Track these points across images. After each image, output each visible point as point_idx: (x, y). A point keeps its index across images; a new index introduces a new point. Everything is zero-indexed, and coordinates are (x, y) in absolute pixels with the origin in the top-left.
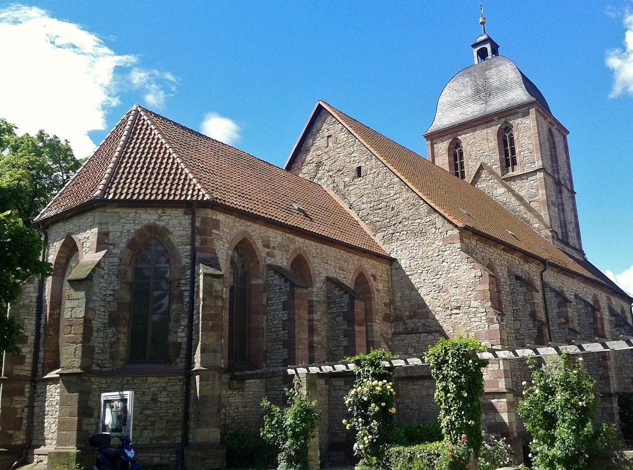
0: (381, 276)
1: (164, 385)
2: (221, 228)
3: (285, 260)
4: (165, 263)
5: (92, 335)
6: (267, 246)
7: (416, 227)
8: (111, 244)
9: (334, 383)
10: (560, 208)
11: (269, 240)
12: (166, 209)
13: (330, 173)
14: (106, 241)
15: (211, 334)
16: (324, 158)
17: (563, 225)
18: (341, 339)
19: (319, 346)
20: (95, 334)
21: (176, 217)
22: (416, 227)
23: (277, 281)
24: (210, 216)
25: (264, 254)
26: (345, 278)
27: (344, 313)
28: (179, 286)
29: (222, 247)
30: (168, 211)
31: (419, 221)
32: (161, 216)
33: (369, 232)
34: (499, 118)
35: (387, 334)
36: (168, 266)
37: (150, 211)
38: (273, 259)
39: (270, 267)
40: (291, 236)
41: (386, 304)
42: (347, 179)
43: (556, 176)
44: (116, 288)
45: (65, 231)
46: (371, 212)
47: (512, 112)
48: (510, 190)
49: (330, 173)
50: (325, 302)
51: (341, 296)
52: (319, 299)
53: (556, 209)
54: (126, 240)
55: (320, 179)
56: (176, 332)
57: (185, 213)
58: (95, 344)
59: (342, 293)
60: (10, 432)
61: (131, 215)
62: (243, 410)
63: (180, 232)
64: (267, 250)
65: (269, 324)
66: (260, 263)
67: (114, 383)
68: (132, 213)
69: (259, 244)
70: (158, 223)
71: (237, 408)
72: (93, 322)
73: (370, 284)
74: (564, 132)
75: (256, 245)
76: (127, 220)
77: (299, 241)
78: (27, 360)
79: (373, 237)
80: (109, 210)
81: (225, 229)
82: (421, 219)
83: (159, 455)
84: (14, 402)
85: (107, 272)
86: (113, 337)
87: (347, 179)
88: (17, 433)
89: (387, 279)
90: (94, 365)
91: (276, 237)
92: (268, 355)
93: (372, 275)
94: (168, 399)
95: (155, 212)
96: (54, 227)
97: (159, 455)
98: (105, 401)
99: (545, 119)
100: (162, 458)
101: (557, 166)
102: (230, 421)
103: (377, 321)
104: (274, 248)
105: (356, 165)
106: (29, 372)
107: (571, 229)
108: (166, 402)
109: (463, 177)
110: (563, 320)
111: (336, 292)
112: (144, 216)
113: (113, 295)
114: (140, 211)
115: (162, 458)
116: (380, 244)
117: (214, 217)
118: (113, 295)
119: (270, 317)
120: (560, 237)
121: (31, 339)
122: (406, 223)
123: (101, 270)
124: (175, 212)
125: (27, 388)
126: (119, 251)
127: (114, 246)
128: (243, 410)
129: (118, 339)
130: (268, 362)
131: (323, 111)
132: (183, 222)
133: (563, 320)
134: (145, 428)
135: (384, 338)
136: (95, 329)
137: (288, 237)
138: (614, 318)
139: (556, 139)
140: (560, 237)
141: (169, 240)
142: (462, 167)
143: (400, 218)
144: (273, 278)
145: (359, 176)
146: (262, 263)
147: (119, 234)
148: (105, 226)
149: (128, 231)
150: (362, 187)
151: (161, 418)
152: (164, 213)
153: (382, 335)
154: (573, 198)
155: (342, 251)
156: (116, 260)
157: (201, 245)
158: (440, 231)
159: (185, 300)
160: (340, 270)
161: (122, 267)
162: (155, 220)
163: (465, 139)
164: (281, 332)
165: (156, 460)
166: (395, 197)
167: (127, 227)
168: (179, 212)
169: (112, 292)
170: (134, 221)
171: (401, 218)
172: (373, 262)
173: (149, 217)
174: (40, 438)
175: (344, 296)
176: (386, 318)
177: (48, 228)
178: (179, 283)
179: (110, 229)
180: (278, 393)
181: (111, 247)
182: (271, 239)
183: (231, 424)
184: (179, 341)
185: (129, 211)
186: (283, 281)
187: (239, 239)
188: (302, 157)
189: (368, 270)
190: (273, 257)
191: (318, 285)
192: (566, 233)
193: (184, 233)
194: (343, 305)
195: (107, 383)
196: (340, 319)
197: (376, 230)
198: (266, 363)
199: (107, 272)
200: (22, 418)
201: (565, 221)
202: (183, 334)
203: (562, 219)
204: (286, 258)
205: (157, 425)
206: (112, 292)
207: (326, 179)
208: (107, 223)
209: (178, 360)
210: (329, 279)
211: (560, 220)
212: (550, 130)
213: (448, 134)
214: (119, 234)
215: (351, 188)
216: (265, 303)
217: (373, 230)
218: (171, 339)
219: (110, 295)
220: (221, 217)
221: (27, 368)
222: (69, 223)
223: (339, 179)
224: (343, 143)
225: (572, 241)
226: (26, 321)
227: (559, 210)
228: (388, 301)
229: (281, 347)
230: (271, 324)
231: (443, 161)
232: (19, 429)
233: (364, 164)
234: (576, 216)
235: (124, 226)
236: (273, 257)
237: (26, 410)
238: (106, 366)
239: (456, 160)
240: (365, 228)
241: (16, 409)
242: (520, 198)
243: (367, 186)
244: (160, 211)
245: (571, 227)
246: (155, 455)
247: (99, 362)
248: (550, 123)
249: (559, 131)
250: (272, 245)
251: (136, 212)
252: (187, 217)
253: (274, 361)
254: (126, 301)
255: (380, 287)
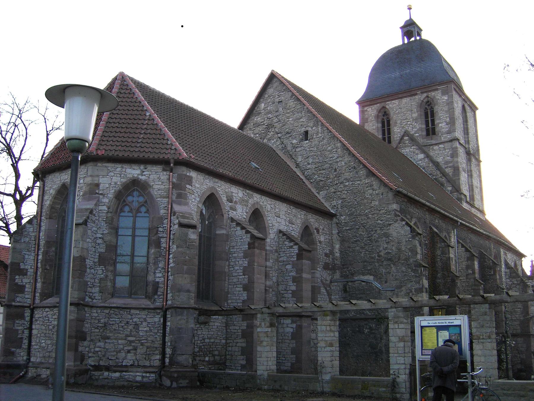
0: (323, 230)
1: (144, 317)
2: (193, 184)
3: (245, 213)
4: (145, 212)
5: (86, 272)
6: (230, 200)
7: (355, 188)
8: (101, 194)
9: (282, 322)
10: (469, 174)
11: (232, 196)
12: (147, 166)
13: (279, 135)
14: (97, 191)
15: (186, 276)
16: (275, 121)
17: (471, 189)
18: (290, 284)
19: (271, 290)
20: (88, 270)
21: (156, 172)
22: (355, 188)
23: (239, 232)
24: (184, 173)
25: (228, 208)
26: (293, 230)
27: (293, 261)
28: (157, 233)
29: (193, 200)
30: (149, 167)
31: (359, 182)
32: (144, 172)
33: (314, 190)
34: (422, 93)
35: (326, 280)
36: (148, 215)
37: (135, 167)
38: (235, 213)
39: (232, 220)
40: (251, 193)
41: (326, 255)
42: (294, 141)
43: (467, 146)
44: (105, 232)
45: (61, 180)
46: (315, 172)
47: (413, 93)
48: (428, 156)
49: (279, 135)
50: (276, 251)
51: (291, 247)
52: (272, 249)
53: (466, 175)
54: (113, 191)
55: (269, 140)
56: (155, 273)
57: (164, 170)
58: (88, 280)
59: (292, 244)
60: (13, 349)
61: (118, 169)
62: (208, 341)
63: (159, 186)
64: (230, 204)
65: (230, 269)
66: (225, 215)
67: (103, 312)
68: (119, 168)
69: (224, 199)
70: (140, 177)
71: (204, 339)
72: (87, 260)
73: (314, 236)
74: (474, 108)
75: (222, 199)
76: (115, 174)
77: (257, 198)
78: (26, 290)
79: (317, 195)
80: (99, 164)
81: (197, 185)
82: (360, 181)
83: (141, 374)
84: (16, 325)
85: (97, 218)
86: (102, 274)
87: (294, 141)
88: (18, 351)
89: (328, 233)
90: (87, 297)
91: (238, 193)
92: (229, 296)
93: (316, 229)
94: (148, 329)
95: (138, 168)
96: (50, 177)
97: (141, 374)
98: (340, 375)
99: (460, 96)
100: (143, 377)
101: (465, 138)
102: (198, 349)
103: (318, 269)
104: (236, 203)
105: (303, 129)
106: (29, 300)
107: (477, 192)
108: (146, 331)
109: (390, 142)
110: (470, 272)
111: (286, 243)
112: (129, 171)
113: (102, 238)
114: (125, 166)
115: (143, 377)
116: (323, 201)
117: (188, 174)
118: (102, 238)
119: (232, 264)
120: (468, 199)
121: (31, 272)
122: (347, 184)
123: (93, 217)
124: (155, 168)
125: (27, 313)
126: (107, 201)
127: (104, 196)
128: (208, 341)
129: (107, 276)
130: (230, 301)
131: (275, 80)
132: (162, 178)
133: (470, 272)
134: (129, 352)
135: (323, 284)
136: (88, 266)
137: (248, 193)
138: (508, 271)
139: (468, 114)
140: (468, 199)
141: (149, 192)
142: (389, 133)
143: (342, 179)
144: (235, 229)
145: (306, 140)
146: (226, 216)
147: (107, 186)
148: (97, 179)
149: (116, 183)
150: (308, 150)
151: (142, 344)
152: (146, 169)
153: (322, 281)
154: (479, 165)
155: (292, 207)
156: (105, 208)
157: (176, 198)
158: (377, 192)
159: (162, 245)
160: (289, 223)
161: (110, 215)
162: (139, 175)
163: (392, 106)
164: (241, 277)
165: (139, 379)
166: (338, 160)
167: (115, 179)
168: (158, 169)
169: (101, 236)
170: (121, 175)
171: (342, 179)
172: (317, 217)
173: (133, 172)
174: (38, 356)
175: (294, 247)
176: (326, 267)
177: (45, 177)
178: (157, 231)
179: (100, 181)
180: (237, 328)
181: (101, 197)
182: (234, 194)
183: (198, 352)
184: (157, 280)
185: (117, 166)
186: (244, 233)
187: (208, 193)
188: (254, 119)
189: (312, 224)
190: (235, 210)
191: (272, 236)
192: (473, 196)
193: (163, 187)
194: (293, 254)
195: (97, 313)
196: (289, 267)
197: (320, 189)
198: (227, 303)
199: (97, 218)
200: (22, 338)
201: (472, 185)
202: (160, 275)
203: (470, 184)
204: (247, 213)
205: (138, 351)
206: (101, 236)
207: (275, 140)
208: (98, 176)
209: (156, 297)
210: (280, 232)
211: (469, 185)
212: (463, 107)
213: (377, 103)
214: (107, 186)
215: (298, 150)
216: (227, 251)
217: (317, 188)
218: (150, 278)
219: (100, 238)
220: (193, 174)
221: (27, 296)
222: (64, 174)
223: (287, 141)
224: (293, 109)
225: (477, 203)
226: (26, 257)
227: (468, 175)
228: (328, 252)
229: (242, 289)
230: (232, 269)
231: (373, 127)
232: (20, 347)
233: (310, 129)
234: (481, 181)
235: (112, 179)
236: (235, 210)
237: (26, 332)
238: (96, 298)
239: (383, 126)
240: (309, 186)
241: (18, 330)
242: (437, 165)
243: (313, 149)
244: (142, 167)
245: (476, 191)
246: (138, 374)
247: (91, 294)
248: (464, 100)
249: (471, 108)
250: (235, 200)
251: (123, 167)
252: (165, 173)
253: (234, 301)
254: (113, 244)
255: (322, 239)
